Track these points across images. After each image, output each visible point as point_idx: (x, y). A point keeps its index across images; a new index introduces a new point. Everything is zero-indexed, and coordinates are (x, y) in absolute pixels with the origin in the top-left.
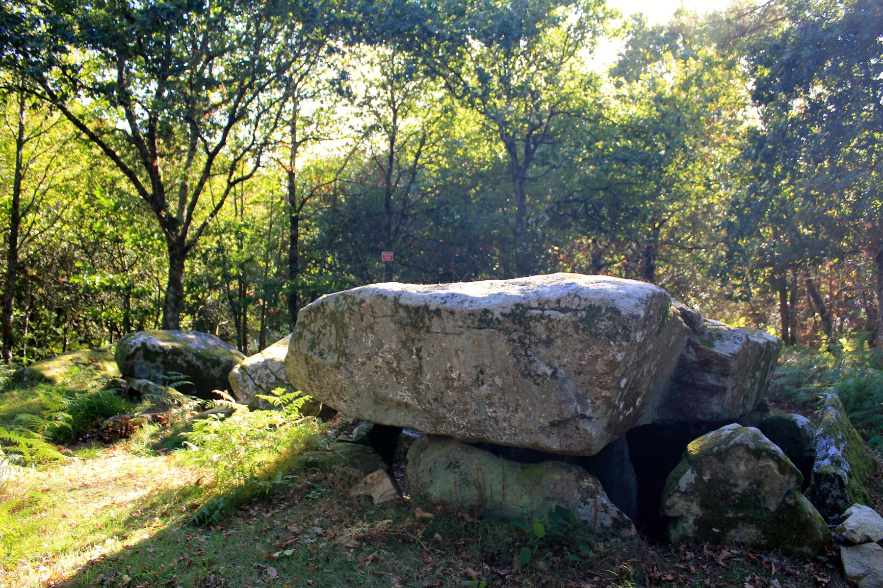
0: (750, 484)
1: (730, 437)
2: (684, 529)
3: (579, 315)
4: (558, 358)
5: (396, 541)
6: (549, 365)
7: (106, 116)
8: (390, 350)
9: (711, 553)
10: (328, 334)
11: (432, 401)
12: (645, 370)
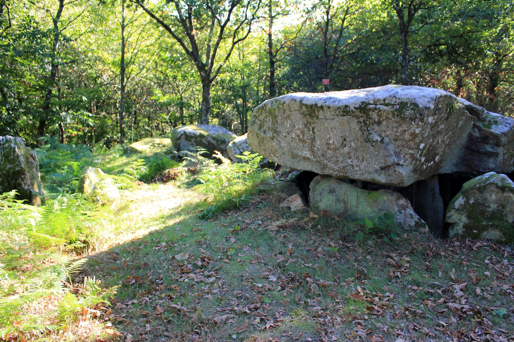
0: (498, 207)
1: (488, 179)
2: (457, 230)
3: (395, 107)
4: (384, 131)
5: (298, 228)
6: (380, 135)
7: (166, 9)
8: (299, 129)
9: (470, 243)
10: (268, 121)
11: (320, 156)
12: (440, 140)
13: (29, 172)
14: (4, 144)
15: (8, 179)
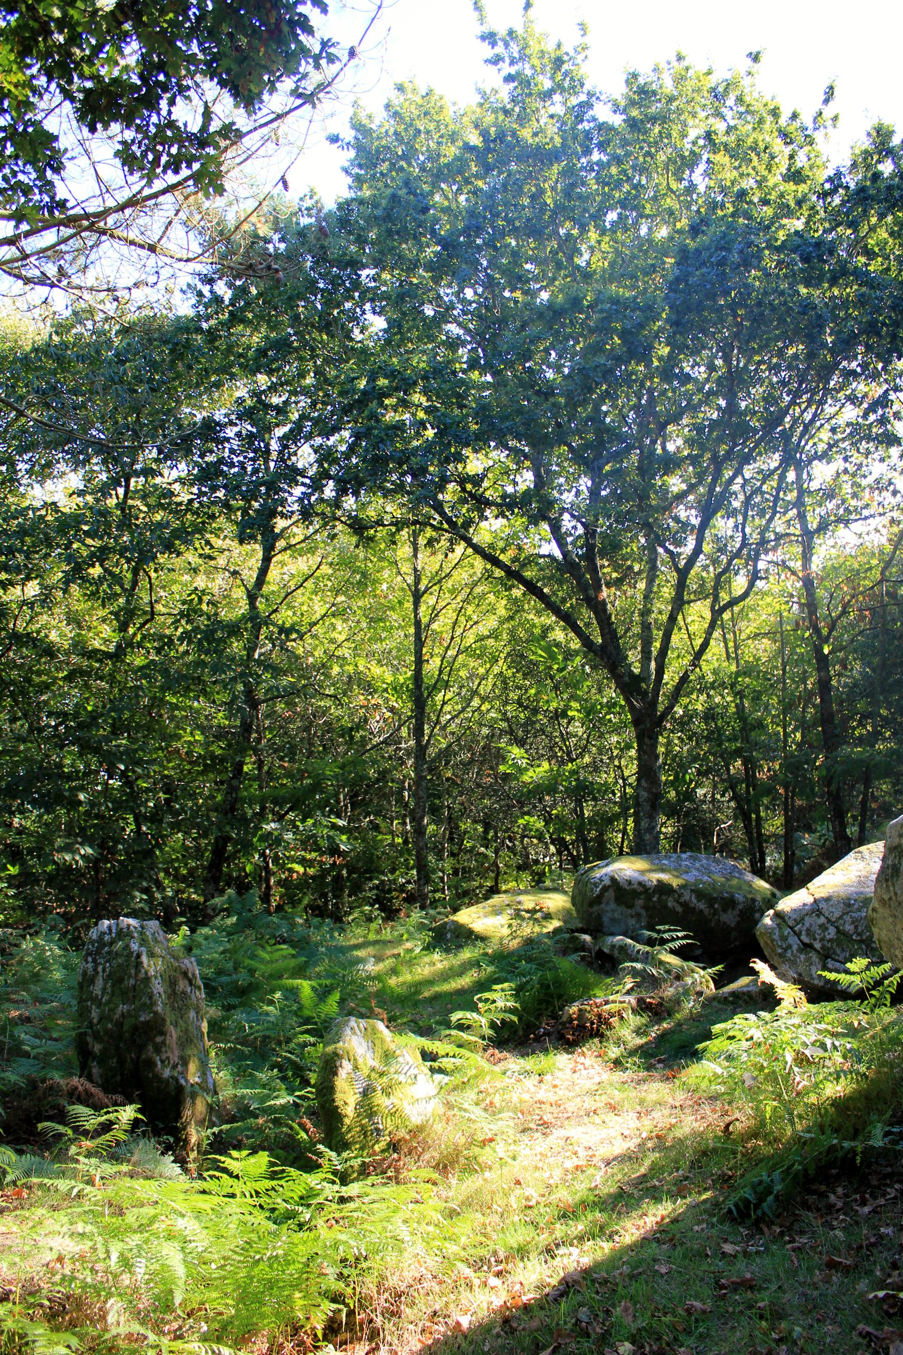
13: (176, 1026)
14: (112, 943)
15: (118, 1048)
